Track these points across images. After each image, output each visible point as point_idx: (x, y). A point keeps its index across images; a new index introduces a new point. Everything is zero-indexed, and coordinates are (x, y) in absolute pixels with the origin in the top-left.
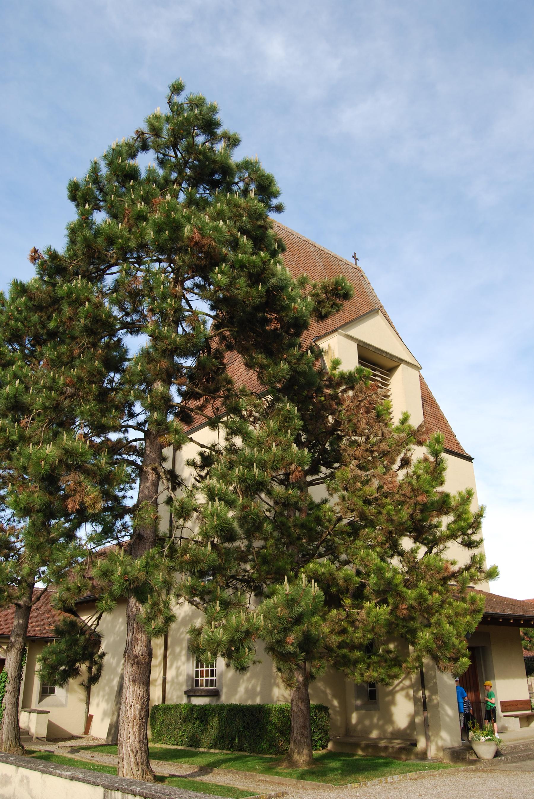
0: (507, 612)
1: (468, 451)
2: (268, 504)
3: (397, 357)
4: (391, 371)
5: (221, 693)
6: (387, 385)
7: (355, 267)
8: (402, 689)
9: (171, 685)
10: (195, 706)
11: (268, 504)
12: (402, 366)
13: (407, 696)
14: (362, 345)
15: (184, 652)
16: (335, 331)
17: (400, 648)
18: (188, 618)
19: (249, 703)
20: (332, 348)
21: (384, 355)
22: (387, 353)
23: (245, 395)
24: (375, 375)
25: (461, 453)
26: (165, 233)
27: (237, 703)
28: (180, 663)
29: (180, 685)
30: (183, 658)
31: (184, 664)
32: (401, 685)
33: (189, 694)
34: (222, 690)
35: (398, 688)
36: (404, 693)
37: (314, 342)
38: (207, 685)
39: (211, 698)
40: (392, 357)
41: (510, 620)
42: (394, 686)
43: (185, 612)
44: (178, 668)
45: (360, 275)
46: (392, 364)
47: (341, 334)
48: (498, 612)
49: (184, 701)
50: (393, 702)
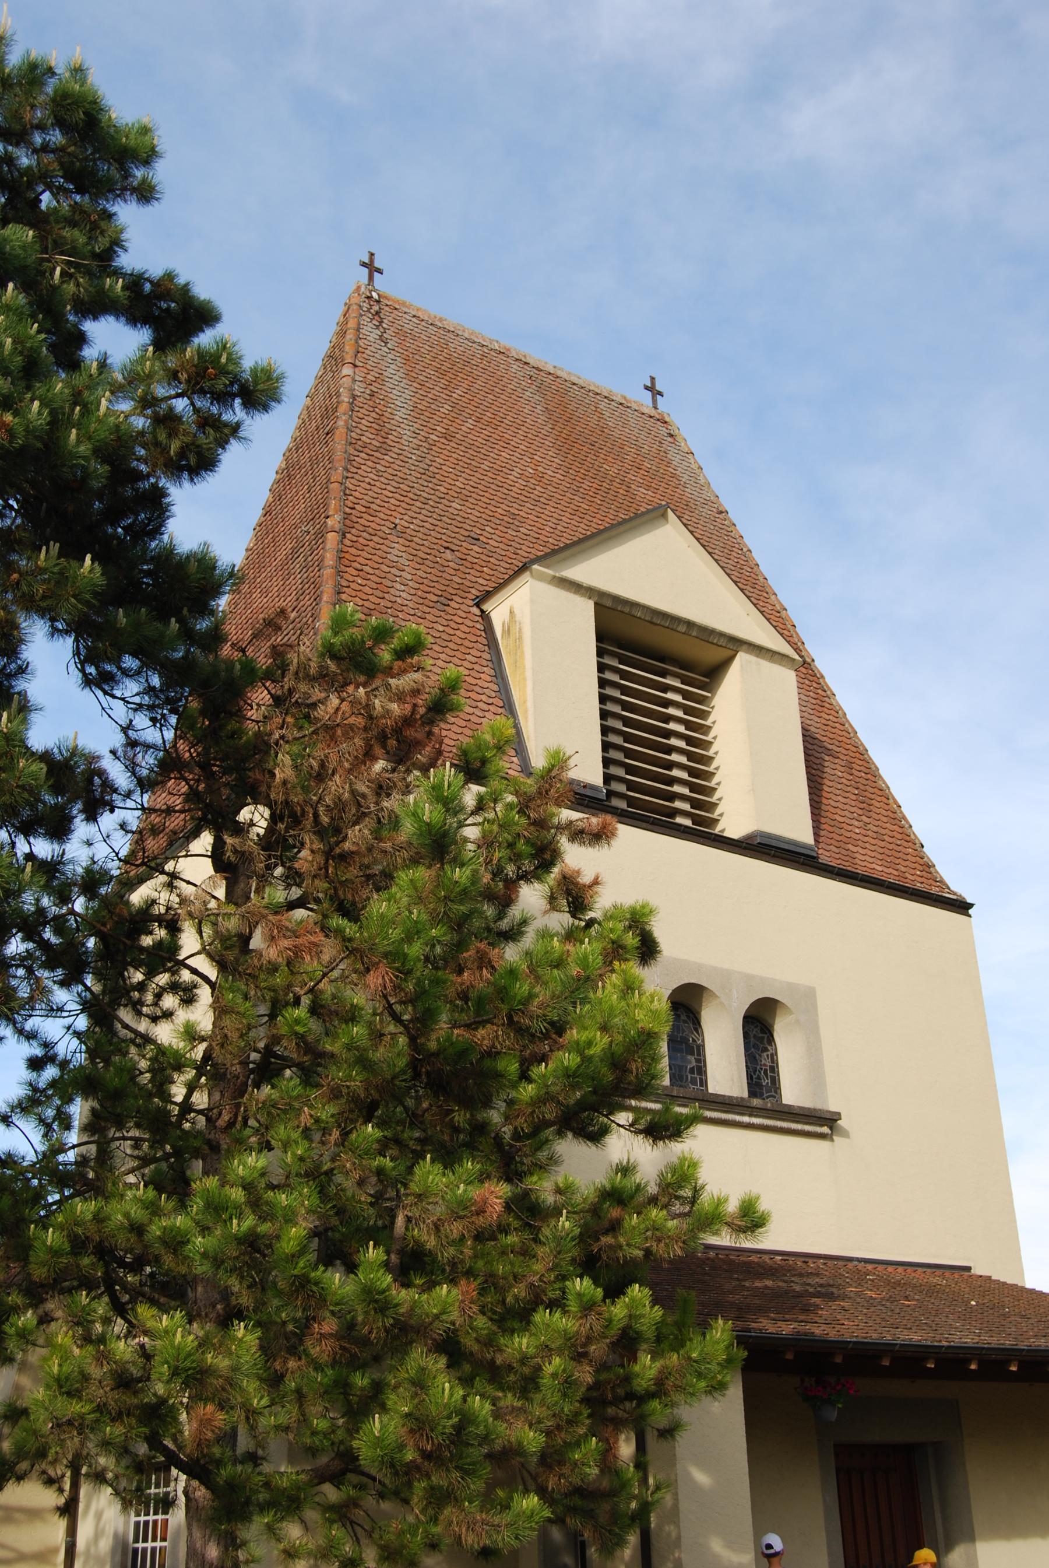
0: (963, 1335)
1: (958, 885)
3: (722, 635)
4: (712, 674)
6: (704, 715)
7: (653, 412)
10: (749, 1091)
12: (742, 659)
14: (608, 603)
16: (524, 568)
20: (518, 617)
21: (682, 628)
22: (690, 624)
23: (287, 742)
24: (666, 688)
25: (934, 890)
26: (136, 390)
37: (478, 605)
40: (706, 634)
41: (969, 1361)
45: (664, 431)
46: (710, 655)
47: (541, 577)
48: (916, 1337)
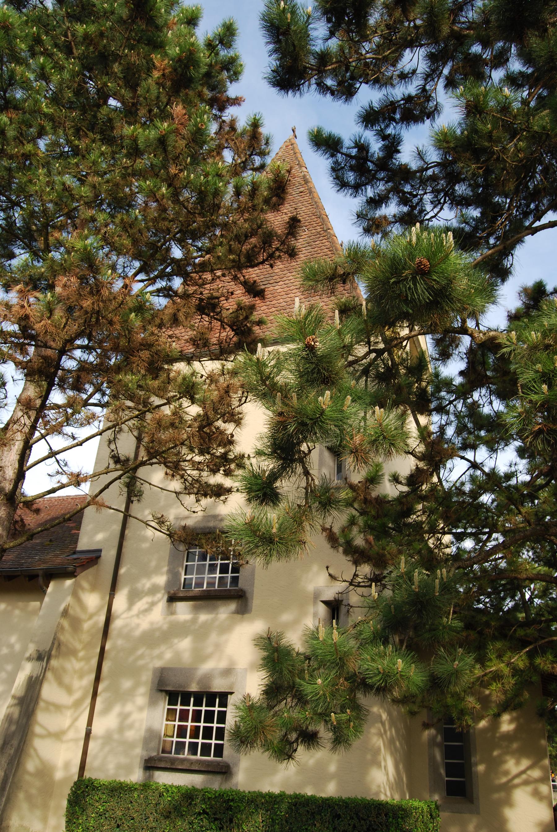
2: (116, 479)
5: (234, 770)
8: (526, 783)
9: (104, 745)
11: (116, 479)
13: (536, 794)
15: (142, 690)
17: (522, 720)
18: (157, 634)
19: (309, 792)
27: (276, 791)
28: (129, 707)
29: (131, 745)
30: (141, 699)
31: (141, 709)
32: (524, 776)
33: (150, 765)
34: (237, 764)
35: (517, 781)
36: (529, 789)
38: (177, 752)
39: (209, 777)
42: (510, 777)
43: (152, 623)
44: (124, 717)
49: (136, 776)
50: (508, 802)
